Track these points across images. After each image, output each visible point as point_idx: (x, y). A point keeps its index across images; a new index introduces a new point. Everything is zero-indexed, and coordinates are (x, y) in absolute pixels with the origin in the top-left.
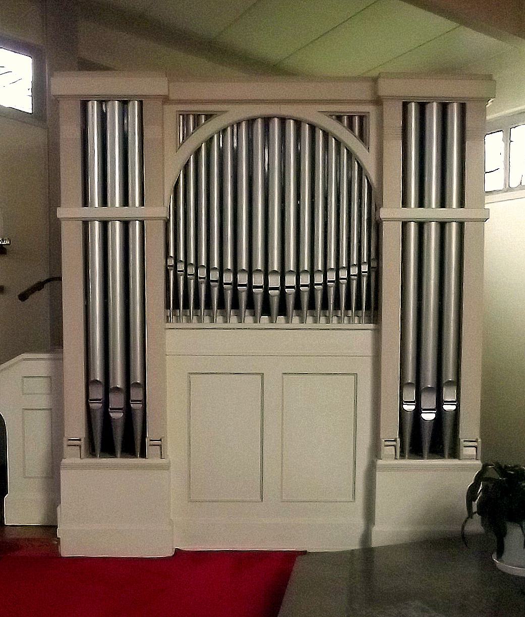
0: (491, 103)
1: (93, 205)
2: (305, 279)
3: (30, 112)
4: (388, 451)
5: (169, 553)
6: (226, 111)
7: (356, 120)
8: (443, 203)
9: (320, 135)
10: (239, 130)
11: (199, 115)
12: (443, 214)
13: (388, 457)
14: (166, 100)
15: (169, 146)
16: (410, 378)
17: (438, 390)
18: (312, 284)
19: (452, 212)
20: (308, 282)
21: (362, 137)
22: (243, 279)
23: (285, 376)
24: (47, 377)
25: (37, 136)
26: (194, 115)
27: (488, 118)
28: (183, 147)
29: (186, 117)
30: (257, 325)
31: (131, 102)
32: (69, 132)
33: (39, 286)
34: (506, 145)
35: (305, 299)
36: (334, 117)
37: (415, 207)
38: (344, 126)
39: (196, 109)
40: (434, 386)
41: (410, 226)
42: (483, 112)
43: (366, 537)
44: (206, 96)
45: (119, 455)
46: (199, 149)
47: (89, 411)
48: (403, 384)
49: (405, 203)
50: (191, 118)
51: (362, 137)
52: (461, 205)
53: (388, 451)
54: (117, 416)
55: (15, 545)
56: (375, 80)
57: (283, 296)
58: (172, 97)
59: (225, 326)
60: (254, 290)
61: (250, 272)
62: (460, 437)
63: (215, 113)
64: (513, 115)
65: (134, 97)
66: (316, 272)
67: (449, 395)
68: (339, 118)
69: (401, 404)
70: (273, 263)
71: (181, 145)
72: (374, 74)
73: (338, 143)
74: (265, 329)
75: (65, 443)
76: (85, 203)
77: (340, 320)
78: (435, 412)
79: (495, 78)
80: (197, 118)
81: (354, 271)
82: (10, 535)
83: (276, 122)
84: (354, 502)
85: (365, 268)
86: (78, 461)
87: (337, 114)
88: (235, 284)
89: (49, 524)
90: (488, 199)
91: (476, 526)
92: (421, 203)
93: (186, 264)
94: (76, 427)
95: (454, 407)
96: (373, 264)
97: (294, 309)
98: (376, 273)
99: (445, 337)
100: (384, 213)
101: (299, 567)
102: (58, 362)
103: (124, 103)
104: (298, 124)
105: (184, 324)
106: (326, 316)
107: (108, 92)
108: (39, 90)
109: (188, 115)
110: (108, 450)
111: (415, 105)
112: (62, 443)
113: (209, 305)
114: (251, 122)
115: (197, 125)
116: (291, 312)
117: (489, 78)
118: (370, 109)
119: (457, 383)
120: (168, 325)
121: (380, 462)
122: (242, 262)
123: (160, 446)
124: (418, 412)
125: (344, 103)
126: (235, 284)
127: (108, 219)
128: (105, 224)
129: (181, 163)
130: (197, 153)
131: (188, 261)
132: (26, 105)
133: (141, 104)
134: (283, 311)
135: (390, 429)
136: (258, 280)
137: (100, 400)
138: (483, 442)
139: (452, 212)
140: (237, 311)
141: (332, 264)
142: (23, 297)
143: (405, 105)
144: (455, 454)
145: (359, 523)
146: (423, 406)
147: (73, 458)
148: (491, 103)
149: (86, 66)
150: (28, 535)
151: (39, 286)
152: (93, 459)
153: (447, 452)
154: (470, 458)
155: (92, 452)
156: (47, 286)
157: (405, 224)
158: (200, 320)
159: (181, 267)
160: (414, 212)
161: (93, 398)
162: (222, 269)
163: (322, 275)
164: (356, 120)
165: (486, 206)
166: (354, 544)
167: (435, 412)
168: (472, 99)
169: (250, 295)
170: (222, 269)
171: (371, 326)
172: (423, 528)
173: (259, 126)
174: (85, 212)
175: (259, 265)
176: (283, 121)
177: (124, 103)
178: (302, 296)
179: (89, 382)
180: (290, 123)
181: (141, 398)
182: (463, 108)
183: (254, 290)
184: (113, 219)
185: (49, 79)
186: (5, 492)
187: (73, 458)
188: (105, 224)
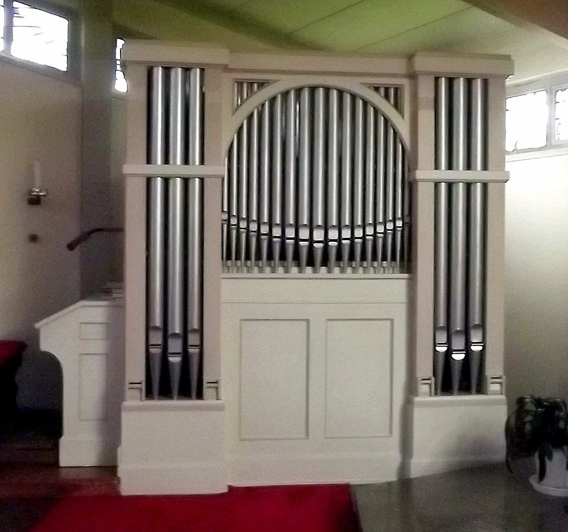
1: (156, 163)
4: (424, 388)
5: (225, 490)
6: (279, 80)
7: (392, 92)
8: (469, 166)
11: (253, 83)
12: (469, 176)
13: (424, 394)
15: (226, 110)
16: (442, 322)
17: (466, 333)
18: (326, 240)
20: (349, 236)
22: (277, 232)
24: (102, 323)
29: (240, 84)
31: (193, 70)
35: (333, 253)
36: (372, 88)
37: (181, 164)
38: (382, 96)
39: (244, 78)
40: (463, 329)
41: (441, 186)
43: (404, 467)
48: (436, 328)
49: (437, 167)
50: (245, 85)
51: (397, 106)
53: (424, 388)
54: (175, 360)
55: (76, 485)
56: (410, 57)
57: (326, 249)
60: (315, 245)
62: (418, 376)
63: (266, 81)
65: (197, 65)
66: (330, 227)
67: (476, 337)
68: (377, 89)
69: (435, 346)
71: (236, 110)
73: (376, 111)
74: (327, 279)
75: (127, 386)
77: (343, 271)
79: (512, 58)
80: (251, 84)
81: (390, 226)
82: (64, 474)
83: (321, 92)
85: (399, 223)
86: (137, 403)
87: (385, 86)
88: (283, 237)
89: (101, 465)
93: (239, 218)
94: (136, 371)
95: (480, 348)
96: (407, 220)
99: (190, 280)
100: (419, 174)
103: (187, 70)
104: (341, 93)
106: (247, 266)
107: (155, 59)
110: (165, 392)
112: (123, 385)
115: (251, 92)
118: (405, 83)
119: (483, 326)
122: (345, 218)
123: (217, 388)
124: (448, 353)
125: (348, 75)
126: (283, 237)
128: (166, 181)
130: (250, 118)
132: (62, 64)
133: (202, 70)
134: (325, 262)
135: (425, 368)
139: (477, 174)
141: (370, 220)
143: (437, 79)
144: (481, 390)
145: (394, 457)
147: (133, 400)
150: (86, 475)
152: (149, 401)
154: (495, 393)
155: (149, 394)
157: (437, 185)
160: (444, 174)
161: (153, 343)
164: (392, 92)
166: (393, 477)
169: (297, 247)
171: (406, 276)
174: (149, 170)
175: (305, 220)
176: (327, 90)
177: (187, 70)
180: (333, 92)
181: (198, 343)
183: (315, 245)
184: (155, 176)
187: (133, 400)
188: (166, 181)
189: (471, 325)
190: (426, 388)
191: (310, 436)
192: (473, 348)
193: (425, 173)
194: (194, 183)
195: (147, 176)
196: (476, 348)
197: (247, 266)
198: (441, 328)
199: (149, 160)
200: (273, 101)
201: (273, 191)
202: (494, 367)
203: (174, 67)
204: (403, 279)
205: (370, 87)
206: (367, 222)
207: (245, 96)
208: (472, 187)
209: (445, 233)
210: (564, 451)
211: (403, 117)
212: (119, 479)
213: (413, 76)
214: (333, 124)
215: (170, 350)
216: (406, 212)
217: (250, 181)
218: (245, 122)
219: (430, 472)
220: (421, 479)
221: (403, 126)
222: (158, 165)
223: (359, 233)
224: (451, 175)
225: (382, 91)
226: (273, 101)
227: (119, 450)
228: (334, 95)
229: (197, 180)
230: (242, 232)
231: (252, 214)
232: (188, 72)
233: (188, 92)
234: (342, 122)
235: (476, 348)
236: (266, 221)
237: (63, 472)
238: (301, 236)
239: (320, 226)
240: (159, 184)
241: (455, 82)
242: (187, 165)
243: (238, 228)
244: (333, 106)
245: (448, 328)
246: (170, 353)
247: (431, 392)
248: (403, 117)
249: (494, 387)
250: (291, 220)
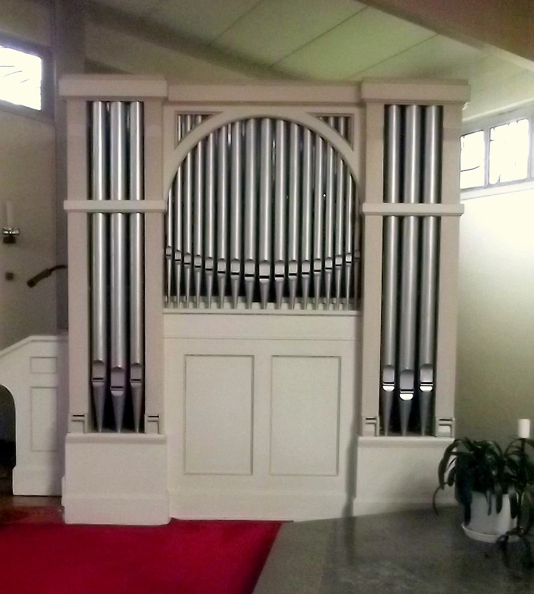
0: (467, 106)
1: (97, 198)
2: (280, 269)
3: (39, 109)
4: (369, 429)
5: (165, 521)
6: (221, 112)
8: (421, 199)
9: (308, 135)
10: (248, 129)
12: (422, 209)
13: (369, 434)
14: (165, 101)
16: (390, 360)
17: (416, 373)
18: (273, 275)
19: (430, 207)
21: (347, 136)
24: (52, 357)
25: (46, 132)
26: (192, 116)
27: (464, 120)
28: (181, 145)
29: (184, 117)
30: (263, 311)
32: (76, 131)
33: (47, 273)
34: (486, 144)
36: (321, 118)
42: (459, 115)
43: (349, 508)
44: (207, 98)
45: (101, 430)
46: (196, 147)
47: (92, 389)
48: (383, 366)
49: (386, 198)
50: (189, 118)
51: (347, 136)
52: (400, 200)
53: (369, 429)
54: (118, 394)
55: (23, 513)
56: (359, 85)
58: (170, 99)
59: (219, 311)
60: (276, 278)
61: (243, 261)
62: (363, 415)
64: (492, 116)
65: (136, 99)
67: (426, 376)
68: (326, 119)
69: (381, 384)
71: (179, 143)
72: (358, 78)
75: (70, 418)
77: (290, 307)
78: (413, 392)
82: (17, 503)
84: (338, 475)
85: (349, 259)
86: (80, 435)
89: (53, 494)
90: (463, 195)
91: (449, 497)
92: (401, 198)
94: (80, 403)
95: (430, 388)
96: (357, 255)
97: (226, 296)
98: (359, 263)
101: (282, 535)
102: (63, 343)
103: (127, 104)
104: (288, 124)
105: (190, 308)
108: (48, 88)
109: (186, 116)
110: (109, 425)
111: (417, 108)
112: (67, 418)
113: (216, 292)
114: (245, 122)
115: (194, 123)
117: (464, 83)
118: (355, 111)
119: (433, 366)
120: (166, 310)
121: (361, 439)
123: (157, 422)
127: (111, 211)
128: (108, 216)
129: (180, 159)
130: (194, 150)
131: (195, 253)
132: (36, 103)
133: (142, 105)
134: (272, 298)
135: (371, 408)
136: (250, 269)
137: (102, 379)
138: (457, 422)
139: (430, 207)
140: (231, 297)
141: (318, 255)
142: (31, 283)
143: (387, 108)
144: (431, 432)
145: (341, 496)
147: (77, 432)
148: (467, 106)
149: (94, 68)
150: (35, 503)
151: (47, 273)
153: (423, 429)
154: (445, 435)
155: (94, 427)
156: (54, 273)
157: (386, 219)
158: (195, 306)
159: (178, 256)
160: (394, 207)
162: (216, 259)
163: (254, 265)
165: (462, 202)
166: (335, 512)
167: (413, 392)
168: (450, 103)
169: (257, 285)
170: (216, 259)
171: (354, 312)
173: (252, 126)
174: (90, 205)
175: (251, 255)
176: (274, 121)
177: (127, 104)
178: (276, 286)
179: (92, 362)
182: (440, 111)
184: (115, 211)
185: (57, 83)
186: (13, 463)
188: (108, 216)
189: (421, 364)
190: (371, 428)
191: (253, 473)
192: (422, 388)
193: (373, 206)
195: (88, 211)
196: (426, 389)
197: (333, 303)
199: (90, 195)
201: (219, 227)
202: (445, 408)
203: (113, 101)
204: (352, 316)
205: (318, 117)
206: (276, 259)
207: (189, 129)
208: (425, 221)
209: (394, 271)
210: (486, 496)
211: (353, 148)
212: (63, 508)
213: (362, 104)
215: (113, 383)
216: (356, 247)
218: (189, 155)
219: (374, 512)
220: (370, 519)
221: (352, 157)
222: (100, 201)
223: (280, 269)
224: (401, 209)
225: (332, 121)
227: (63, 479)
228: (281, 126)
229: (138, 215)
230: (338, 269)
231: (197, 250)
232: (128, 106)
233: (128, 126)
234: (327, 154)
235: (426, 389)
236: (223, 257)
237: (15, 500)
238: (277, 272)
239: (251, 260)
240: (100, 219)
241: (428, 109)
242: (402, 202)
243: (183, 263)
244: (431, 139)
246: (112, 387)
247: (376, 433)
248: (353, 148)
250: (236, 255)
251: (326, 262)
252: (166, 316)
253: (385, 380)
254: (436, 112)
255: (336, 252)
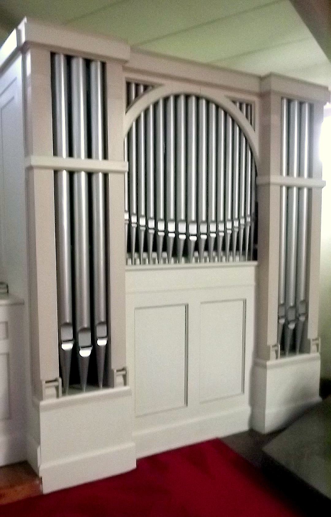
1: (293, 175)
13: (51, 396)
16: (68, 319)
17: (92, 329)
23: (183, 308)
35: (192, 246)
37: (67, 156)
48: (61, 325)
67: (101, 331)
68: (234, 102)
70: (235, 214)
76: (55, 153)
86: (54, 401)
116: (202, 253)
118: (255, 100)
120: (127, 268)
128: (300, 189)
139: (305, 181)
143: (53, 55)
145: (245, 409)
146: (81, 344)
157: (56, 172)
166: (244, 427)
172: (292, 405)
174: (57, 162)
176: (187, 97)
188: (71, 174)
190: (53, 391)
194: (98, 178)
198: (67, 324)
200: (156, 105)
214: (181, 127)
216: (253, 211)
217: (139, 178)
224: (72, 163)
225: (238, 104)
226: (156, 105)
245: (74, 324)
249: (313, 347)
251: (250, 221)
252: (127, 274)
253: (64, 338)
254: (100, 70)
255: (240, 215)
